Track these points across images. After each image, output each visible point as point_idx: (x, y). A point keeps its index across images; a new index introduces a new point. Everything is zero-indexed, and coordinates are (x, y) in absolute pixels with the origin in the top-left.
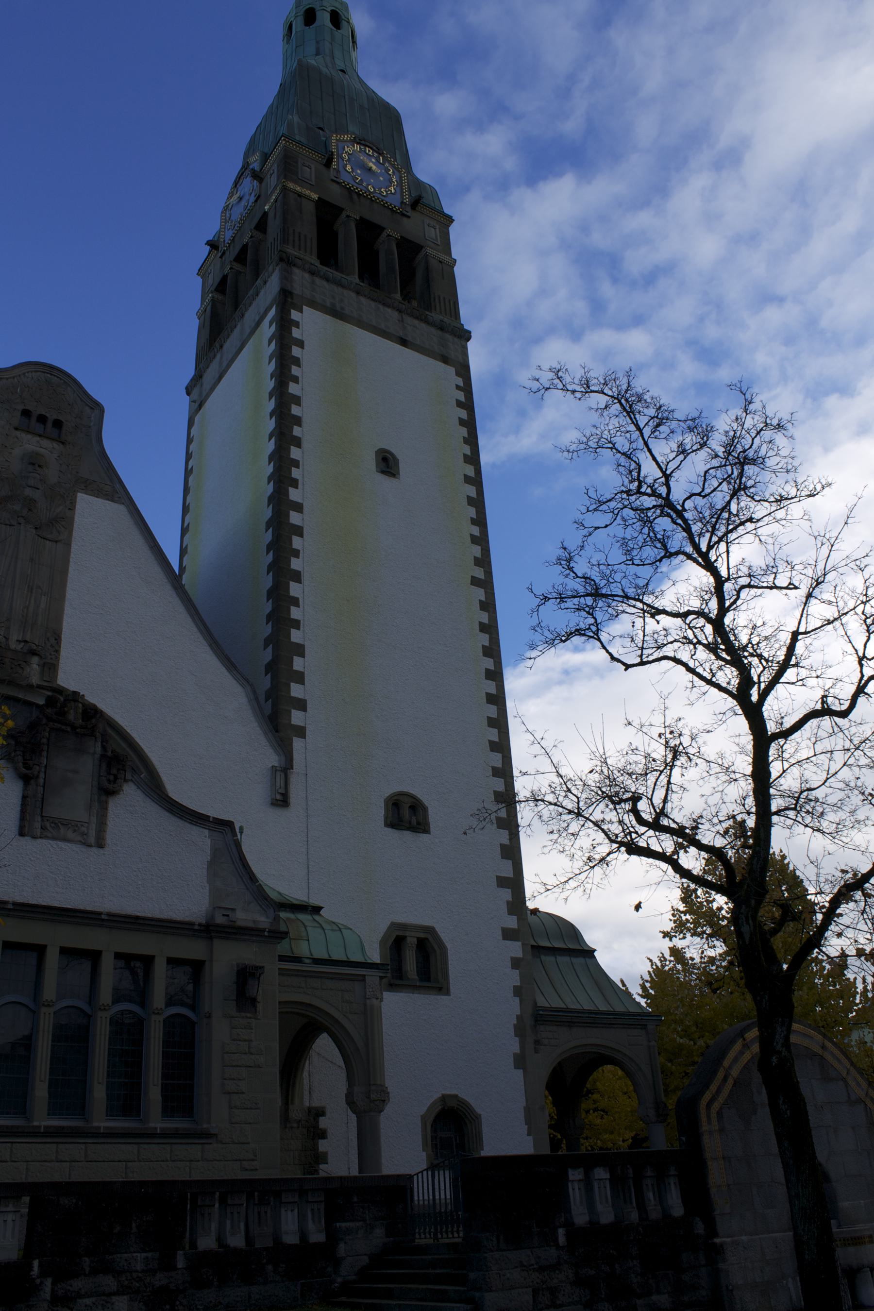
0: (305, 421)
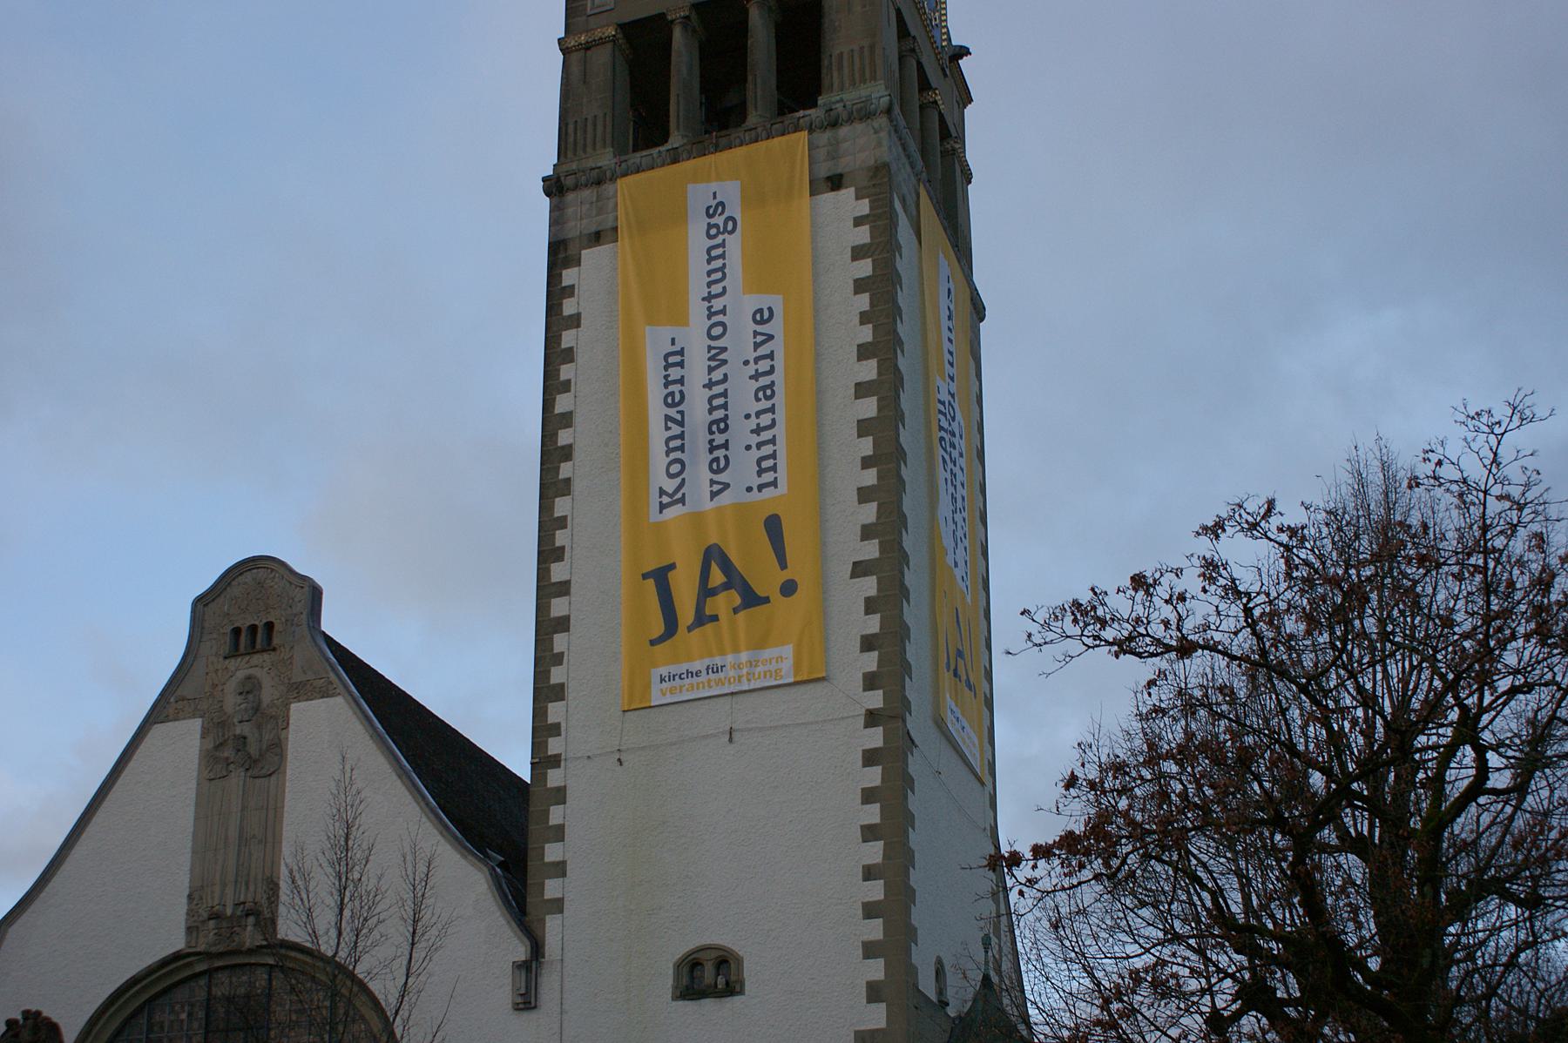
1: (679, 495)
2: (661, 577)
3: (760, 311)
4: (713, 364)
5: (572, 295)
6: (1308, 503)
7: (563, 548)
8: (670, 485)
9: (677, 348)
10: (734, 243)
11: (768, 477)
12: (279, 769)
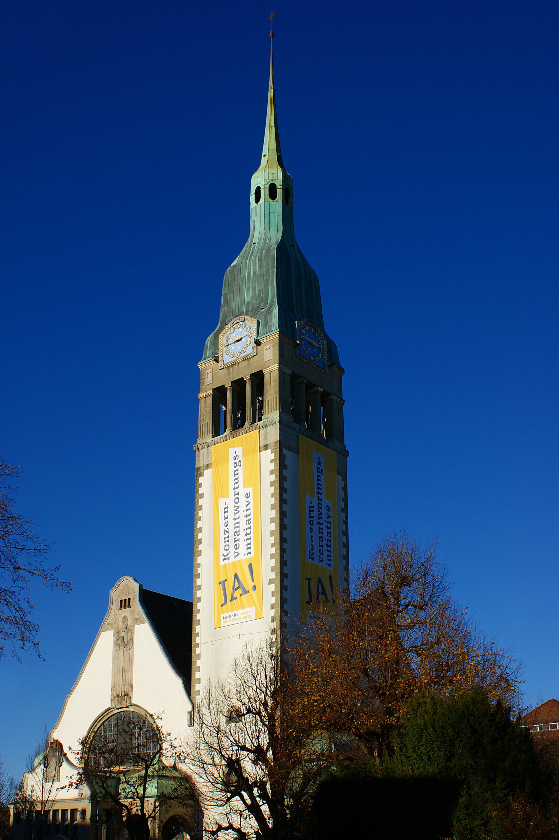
0: (203, 507)
1: (228, 557)
2: (223, 583)
3: (247, 494)
4: (236, 512)
6: (60, 569)
8: (225, 553)
9: (226, 506)
10: (240, 469)
11: (249, 551)
12: (132, 648)
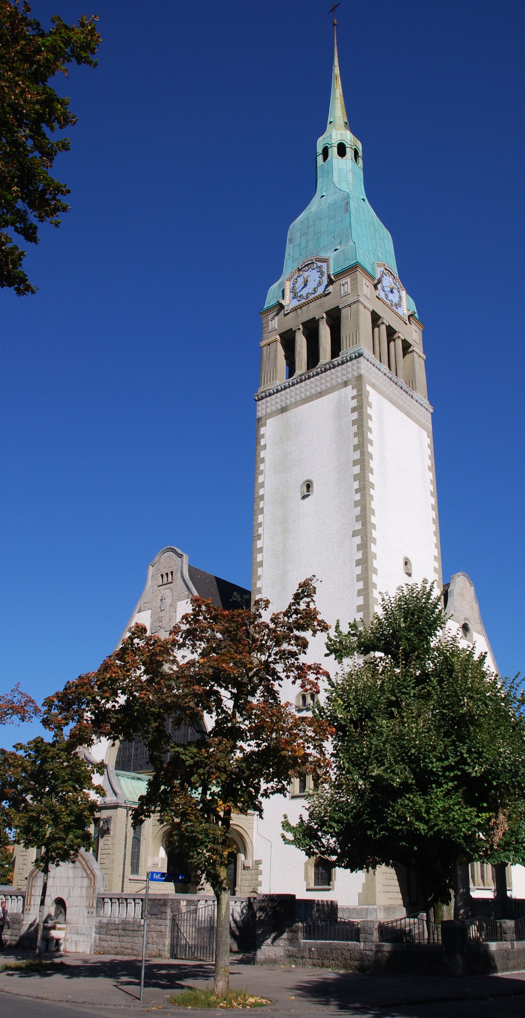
0: (267, 460)
5: (263, 438)
7: (261, 534)
